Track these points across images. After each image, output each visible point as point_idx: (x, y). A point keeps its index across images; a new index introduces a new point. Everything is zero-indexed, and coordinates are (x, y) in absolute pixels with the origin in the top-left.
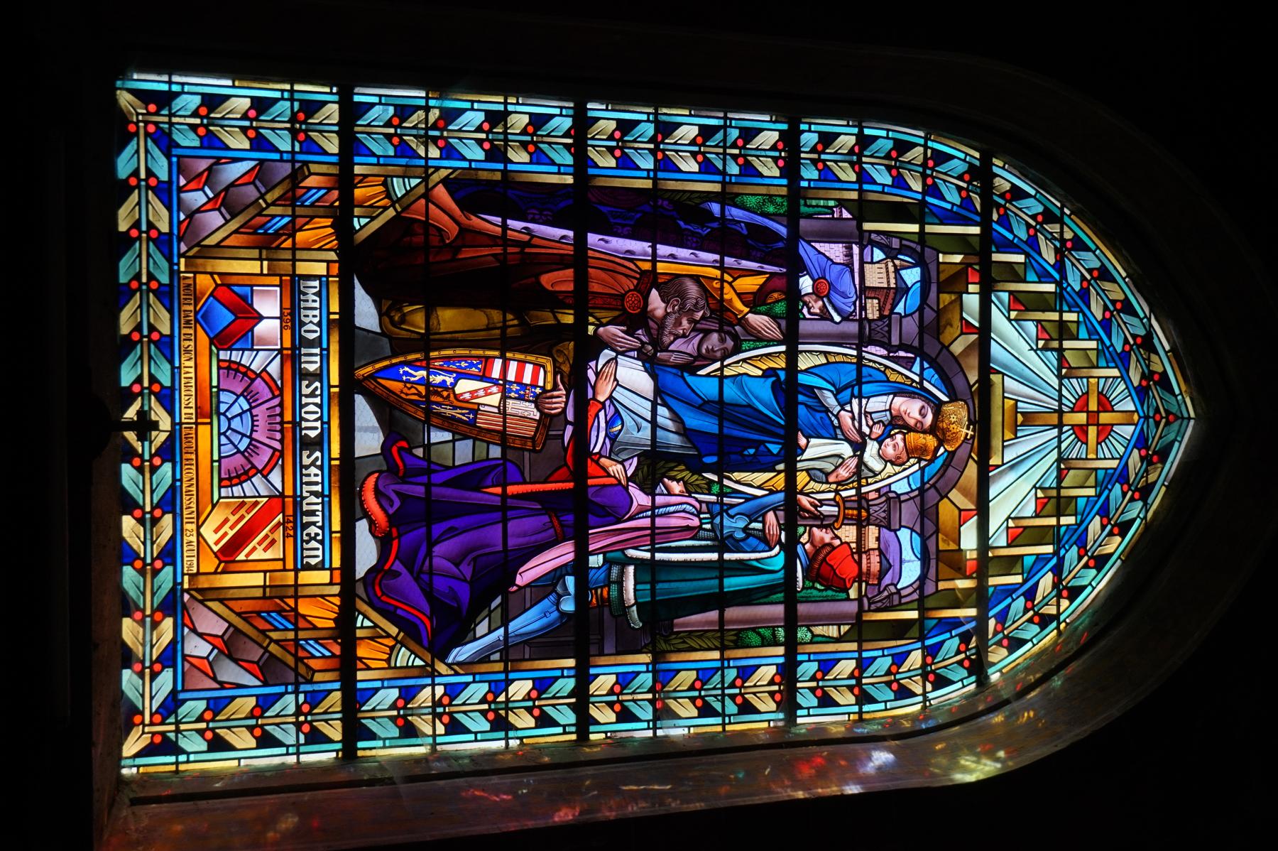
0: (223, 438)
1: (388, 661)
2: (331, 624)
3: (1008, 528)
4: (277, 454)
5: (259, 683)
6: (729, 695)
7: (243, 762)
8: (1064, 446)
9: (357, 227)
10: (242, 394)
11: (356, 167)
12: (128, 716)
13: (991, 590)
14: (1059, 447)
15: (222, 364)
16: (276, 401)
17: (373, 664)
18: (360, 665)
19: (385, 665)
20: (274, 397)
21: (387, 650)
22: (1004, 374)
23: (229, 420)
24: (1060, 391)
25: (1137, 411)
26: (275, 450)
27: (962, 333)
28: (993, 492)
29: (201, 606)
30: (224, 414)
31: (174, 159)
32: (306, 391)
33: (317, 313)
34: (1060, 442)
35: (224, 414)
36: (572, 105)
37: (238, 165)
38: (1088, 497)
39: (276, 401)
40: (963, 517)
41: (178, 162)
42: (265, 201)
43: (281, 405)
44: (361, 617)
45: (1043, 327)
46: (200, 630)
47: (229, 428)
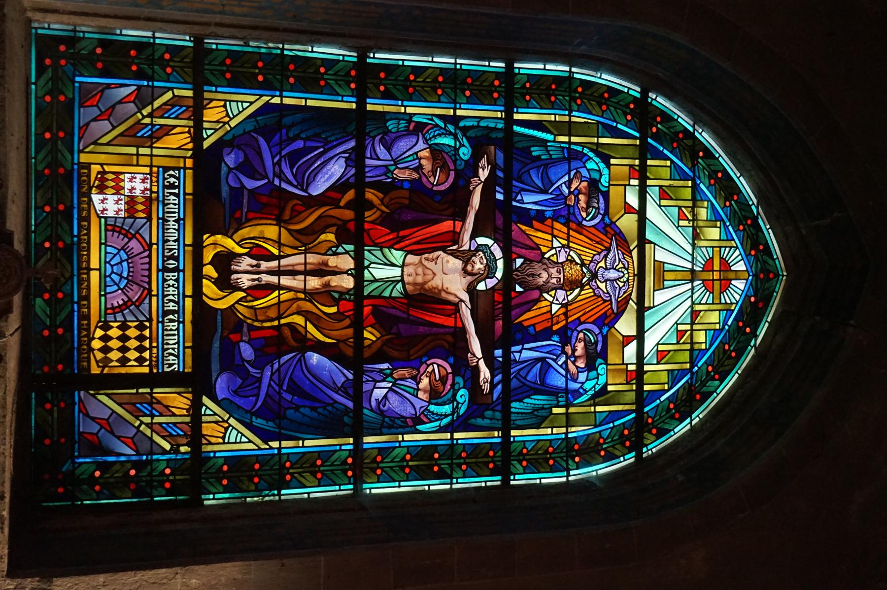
0: (108, 279)
1: (223, 438)
2: (368, 100)
3: (658, 351)
4: (146, 292)
5: (134, 453)
6: (456, 464)
7: (430, 59)
8: (695, 296)
9: (205, 136)
10: (123, 248)
11: (205, 93)
12: (716, 218)
13: (645, 394)
14: (692, 297)
15: (109, 228)
16: (147, 253)
17: (213, 440)
18: (204, 441)
19: (221, 441)
20: (145, 251)
21: (223, 430)
22: (655, 244)
23: (112, 266)
24: (692, 255)
25: (747, 271)
26: (145, 288)
27: (625, 213)
28: (647, 324)
29: (92, 398)
30: (109, 263)
31: (77, 85)
32: (176, 366)
33: (176, 337)
34: (693, 293)
35: (109, 263)
36: (355, 54)
37: (122, 89)
38: (715, 330)
39: (147, 253)
40: (627, 340)
41: (80, 87)
42: (142, 114)
43: (150, 256)
44: (204, 408)
45: (280, 381)
46: (91, 415)
47: (113, 272)
